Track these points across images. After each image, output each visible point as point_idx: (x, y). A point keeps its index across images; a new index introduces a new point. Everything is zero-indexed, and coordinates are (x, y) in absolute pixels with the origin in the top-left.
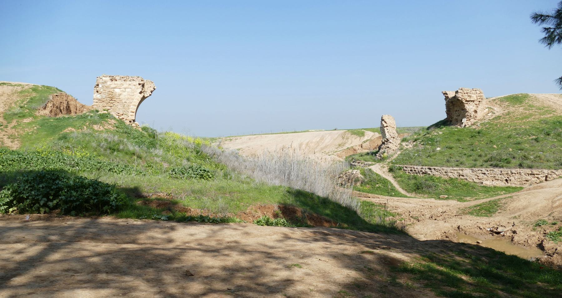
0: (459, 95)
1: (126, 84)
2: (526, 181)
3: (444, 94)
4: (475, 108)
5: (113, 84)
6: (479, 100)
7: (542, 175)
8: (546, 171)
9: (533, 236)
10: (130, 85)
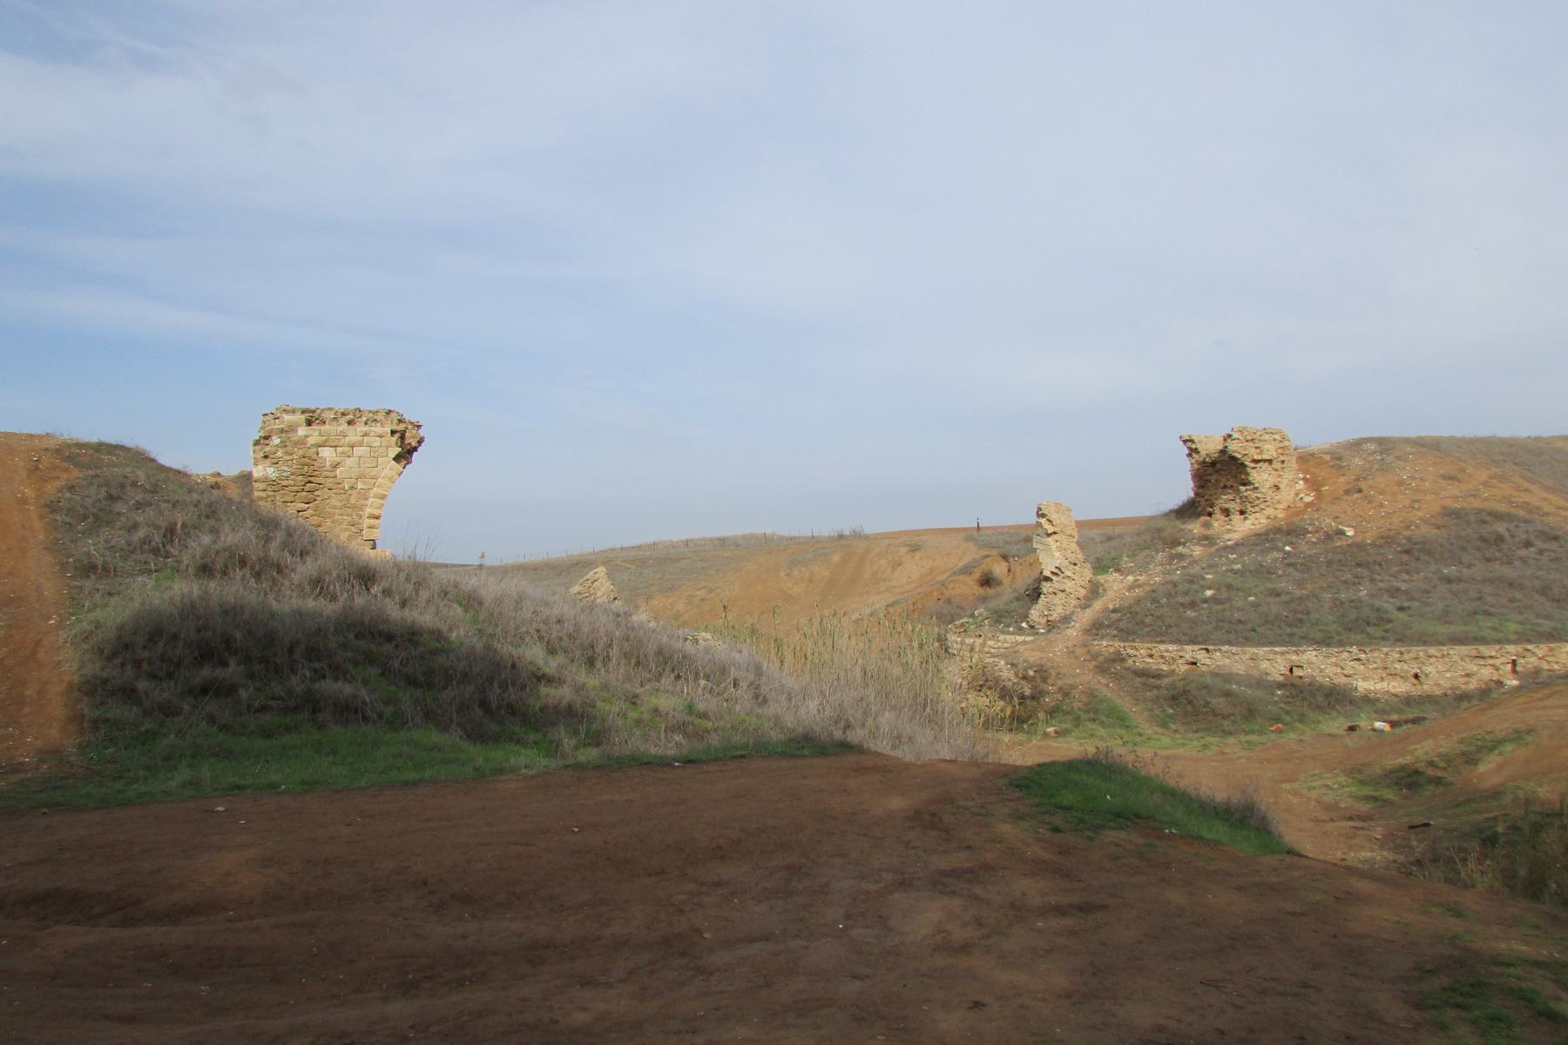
1: (355, 433)
2: (1468, 675)
3: (1185, 442)
4: (1273, 480)
5: (313, 435)
7: (1503, 660)
8: (1511, 648)
9: (139, 506)
10: (366, 435)
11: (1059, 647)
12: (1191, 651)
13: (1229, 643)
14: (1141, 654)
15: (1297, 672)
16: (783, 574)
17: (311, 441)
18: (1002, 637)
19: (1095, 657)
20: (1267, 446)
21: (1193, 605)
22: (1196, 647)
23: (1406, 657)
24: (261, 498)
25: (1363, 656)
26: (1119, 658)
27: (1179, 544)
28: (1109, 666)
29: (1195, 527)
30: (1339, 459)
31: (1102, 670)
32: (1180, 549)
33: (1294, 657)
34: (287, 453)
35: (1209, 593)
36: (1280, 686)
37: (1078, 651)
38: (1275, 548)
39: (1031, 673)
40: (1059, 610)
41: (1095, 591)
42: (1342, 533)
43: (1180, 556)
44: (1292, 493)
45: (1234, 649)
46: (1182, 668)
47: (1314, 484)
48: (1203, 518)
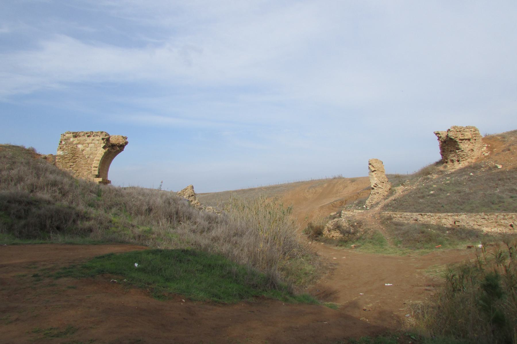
0: (450, 134)
1: (89, 140)
3: (436, 134)
4: (471, 147)
5: (76, 141)
6: (475, 138)
10: (93, 140)
11: (370, 214)
12: (415, 215)
13: (431, 212)
14: (398, 216)
15: (457, 224)
16: (306, 191)
17: (75, 142)
18: (355, 211)
19: (381, 217)
20: (466, 134)
21: (423, 197)
22: (417, 214)
23: (506, 217)
24: (58, 162)
25: (486, 217)
26: (390, 218)
27: (429, 174)
28: (386, 221)
29: (441, 168)
30: (504, 138)
31: (382, 223)
32: (429, 176)
33: (456, 217)
34: (67, 147)
35: (432, 192)
36: (448, 229)
37: (376, 216)
38: (466, 174)
39: (356, 224)
40: (375, 200)
41: (391, 192)
42: (496, 167)
43: (428, 179)
44: (480, 152)
45: (432, 214)
46: (412, 222)
47: (490, 149)
48: (444, 164)
